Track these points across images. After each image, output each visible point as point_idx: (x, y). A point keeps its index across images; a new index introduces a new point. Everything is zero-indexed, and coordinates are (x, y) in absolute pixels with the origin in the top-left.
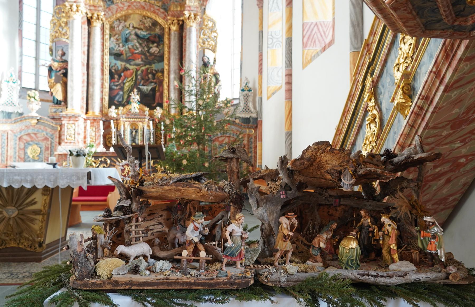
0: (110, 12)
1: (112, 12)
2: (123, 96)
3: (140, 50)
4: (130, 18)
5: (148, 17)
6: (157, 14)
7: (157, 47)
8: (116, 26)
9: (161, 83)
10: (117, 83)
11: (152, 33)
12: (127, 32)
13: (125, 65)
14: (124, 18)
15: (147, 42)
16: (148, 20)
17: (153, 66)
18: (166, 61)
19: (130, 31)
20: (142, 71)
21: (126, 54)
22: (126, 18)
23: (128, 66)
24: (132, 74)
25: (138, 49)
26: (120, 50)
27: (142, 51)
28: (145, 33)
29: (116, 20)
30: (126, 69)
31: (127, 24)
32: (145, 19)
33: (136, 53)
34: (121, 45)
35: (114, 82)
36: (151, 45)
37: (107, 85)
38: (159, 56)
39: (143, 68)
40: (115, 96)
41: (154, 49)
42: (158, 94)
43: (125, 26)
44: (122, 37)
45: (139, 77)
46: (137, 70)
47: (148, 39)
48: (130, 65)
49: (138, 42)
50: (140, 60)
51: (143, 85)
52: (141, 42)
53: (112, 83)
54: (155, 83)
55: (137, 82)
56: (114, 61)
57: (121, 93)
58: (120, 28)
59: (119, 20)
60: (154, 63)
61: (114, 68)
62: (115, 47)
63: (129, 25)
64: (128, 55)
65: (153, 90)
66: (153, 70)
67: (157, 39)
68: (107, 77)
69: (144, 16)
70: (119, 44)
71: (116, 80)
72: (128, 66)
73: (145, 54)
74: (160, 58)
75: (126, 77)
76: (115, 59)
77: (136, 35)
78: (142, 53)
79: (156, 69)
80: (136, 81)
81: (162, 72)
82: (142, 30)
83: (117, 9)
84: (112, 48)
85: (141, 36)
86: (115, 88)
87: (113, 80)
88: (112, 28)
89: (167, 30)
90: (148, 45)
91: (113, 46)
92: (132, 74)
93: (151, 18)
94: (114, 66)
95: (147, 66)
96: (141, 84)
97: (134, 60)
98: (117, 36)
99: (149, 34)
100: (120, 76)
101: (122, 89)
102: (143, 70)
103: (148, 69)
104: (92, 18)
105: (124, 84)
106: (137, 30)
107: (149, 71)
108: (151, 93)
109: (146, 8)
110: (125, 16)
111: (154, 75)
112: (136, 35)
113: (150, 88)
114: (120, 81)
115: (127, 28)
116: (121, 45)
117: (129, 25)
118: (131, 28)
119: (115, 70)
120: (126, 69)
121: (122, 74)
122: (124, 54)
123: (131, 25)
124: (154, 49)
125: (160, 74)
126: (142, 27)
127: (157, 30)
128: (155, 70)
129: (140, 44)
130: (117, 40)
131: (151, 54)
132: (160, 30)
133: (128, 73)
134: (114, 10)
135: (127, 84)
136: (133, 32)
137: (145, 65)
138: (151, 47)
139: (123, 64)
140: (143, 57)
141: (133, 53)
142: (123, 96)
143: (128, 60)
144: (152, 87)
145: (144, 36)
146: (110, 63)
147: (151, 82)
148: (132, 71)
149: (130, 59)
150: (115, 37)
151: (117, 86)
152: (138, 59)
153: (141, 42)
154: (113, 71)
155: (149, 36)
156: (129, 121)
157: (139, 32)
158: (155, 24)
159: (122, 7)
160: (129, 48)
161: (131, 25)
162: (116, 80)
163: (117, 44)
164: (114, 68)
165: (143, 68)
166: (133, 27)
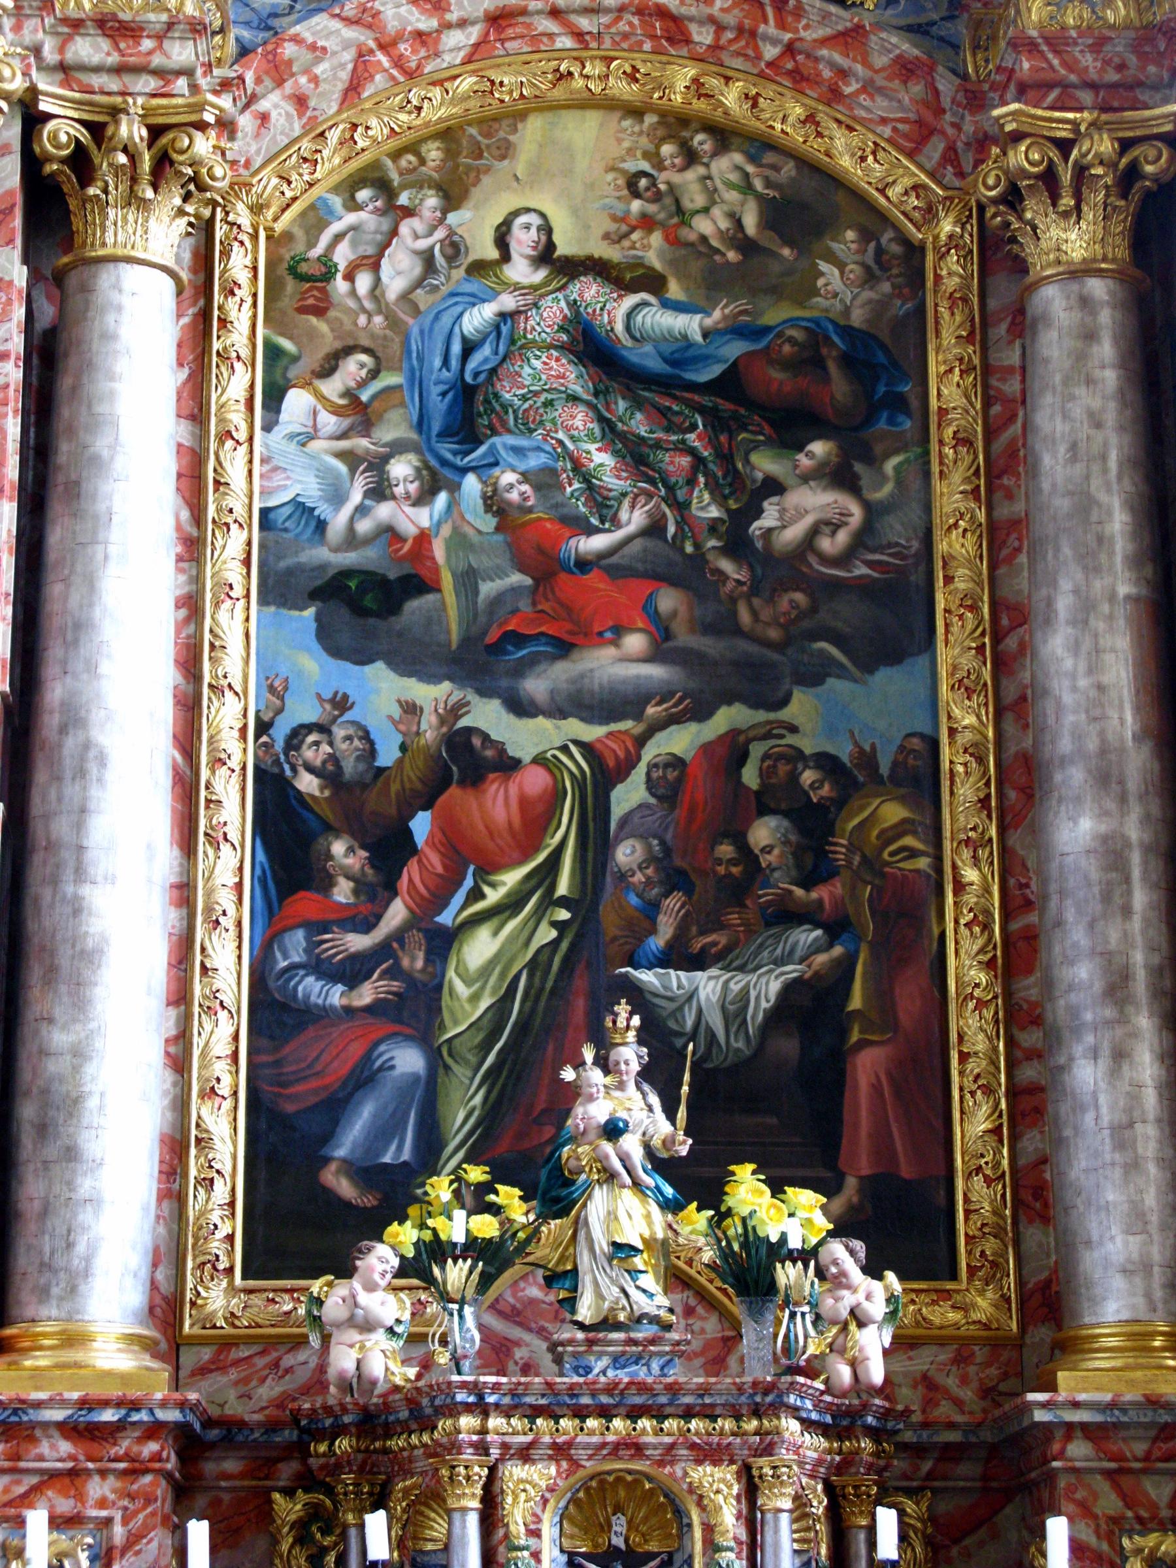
0: (274, 102)
1: (301, 101)
2: (428, 1095)
3: (634, 519)
4: (505, 151)
5: (724, 135)
6: (834, 96)
7: (840, 476)
8: (343, 256)
9: (904, 921)
10: (357, 942)
11: (774, 315)
12: (477, 318)
13: (456, 711)
14: (433, 153)
15: (717, 423)
16: (725, 166)
17: (801, 707)
18: (955, 650)
19: (508, 302)
20: (670, 782)
21: (468, 580)
22: (462, 157)
23: (488, 716)
24: (536, 819)
25: (605, 509)
26: (389, 532)
27: (654, 529)
28: (690, 325)
29: (349, 188)
30: (465, 761)
31: (476, 225)
32: (691, 157)
33: (584, 564)
34: (401, 469)
35: (318, 927)
36: (765, 464)
37: (227, 962)
38: (863, 587)
39: (680, 741)
40: (335, 1108)
41: (804, 509)
42: (868, 1066)
43: (454, 248)
44: (417, 381)
45: (626, 854)
46: (606, 772)
47: (730, 383)
48: (520, 707)
49: (611, 433)
50: (635, 642)
51: (680, 956)
52: (639, 424)
53: (295, 946)
54: (836, 927)
55: (610, 921)
56: (314, 671)
57: (408, 1060)
58: (398, 270)
59: (385, 188)
60: (813, 677)
61: (314, 752)
62: (337, 498)
63: (502, 240)
64: (487, 589)
65: (811, 1008)
66: (797, 756)
67: (840, 387)
68: (229, 867)
69: (676, 124)
70: (378, 464)
71: (343, 892)
72: (488, 716)
73: (690, 574)
74: (888, 614)
75: (468, 857)
76: (329, 640)
77: (588, 345)
78: (664, 560)
79: (844, 751)
80: (585, 902)
81: (920, 777)
82: (653, 283)
83: (362, 53)
84: (301, 508)
85: (648, 359)
86: (336, 996)
87: (305, 903)
88: (298, 283)
89: (952, 272)
90: (725, 458)
91: (300, 484)
92: (536, 819)
93: (760, 146)
94: (323, 729)
95: (725, 718)
96: (657, 943)
97: (564, 648)
98: (354, 367)
99: (736, 330)
100: (390, 851)
101: (416, 1009)
102: (676, 762)
103: (731, 751)
104: (81, 162)
105: (442, 943)
106: (589, 290)
107: (750, 776)
108: (788, 1047)
109: (703, 36)
110: (447, 134)
111: (813, 825)
112: (588, 345)
113: (767, 987)
114: (397, 913)
115: (479, 268)
116: (401, 469)
117: (502, 240)
118: (520, 271)
119: (330, 774)
120: (465, 761)
121: (421, 825)
122: (447, 580)
123: (524, 240)
124: (804, 509)
125: (893, 812)
126: (652, 250)
127: (839, 283)
128: (827, 763)
129: (635, 456)
130: (359, 413)
131: (776, 569)
132: (869, 278)
133: (497, 803)
134: (333, 72)
135: (480, 948)
136: (554, 309)
137: (700, 712)
138: (773, 487)
139: (431, 695)
140: (668, 600)
141: (546, 568)
142: (428, 1095)
143: (487, 657)
144: (792, 971)
145: (681, 354)
146: (276, 691)
147: (787, 916)
148: (535, 781)
149: (518, 639)
150: (332, 387)
151: (352, 972)
152: (619, 631)
153: (639, 424)
154: (307, 783)
155: (735, 349)
156: (560, 1451)
157: (616, 312)
158: (808, 204)
159: (420, 37)
160: (493, 502)
161: (524, 240)
162: (343, 892)
163: (351, 458)
164: (314, 752)
165: (680, 741)
166: (545, 255)
